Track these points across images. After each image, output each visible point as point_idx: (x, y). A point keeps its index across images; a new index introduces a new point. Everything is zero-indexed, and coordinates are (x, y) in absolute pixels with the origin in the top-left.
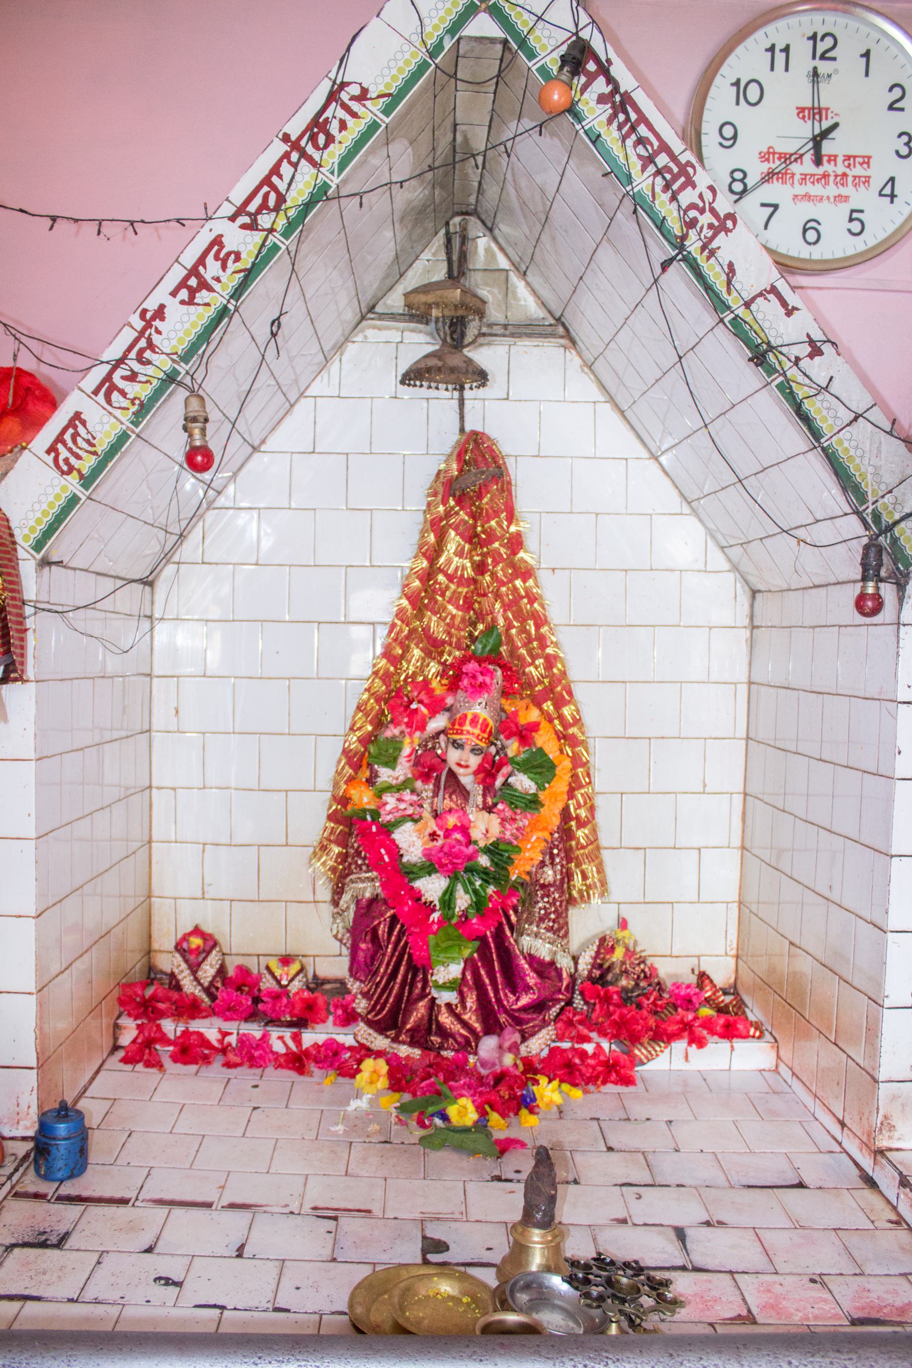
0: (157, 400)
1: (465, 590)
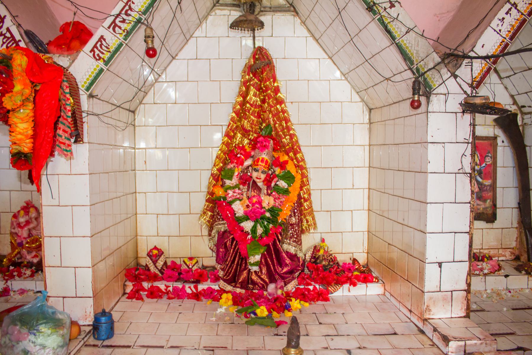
0: (134, 30)
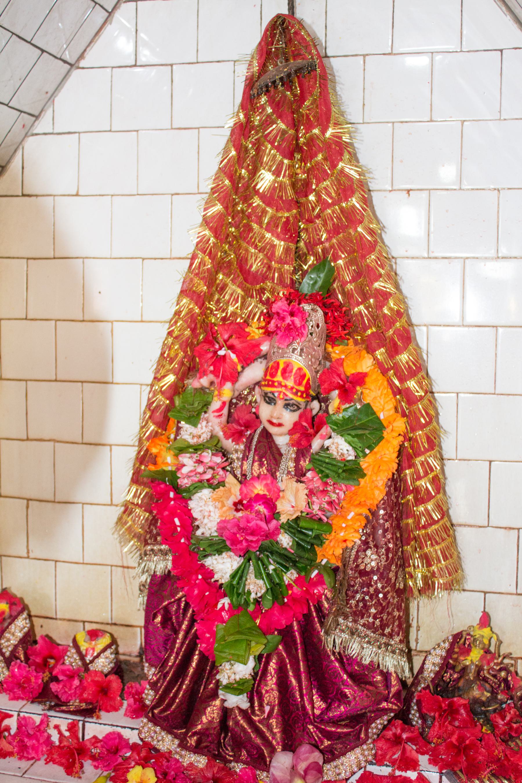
1: (286, 215)
